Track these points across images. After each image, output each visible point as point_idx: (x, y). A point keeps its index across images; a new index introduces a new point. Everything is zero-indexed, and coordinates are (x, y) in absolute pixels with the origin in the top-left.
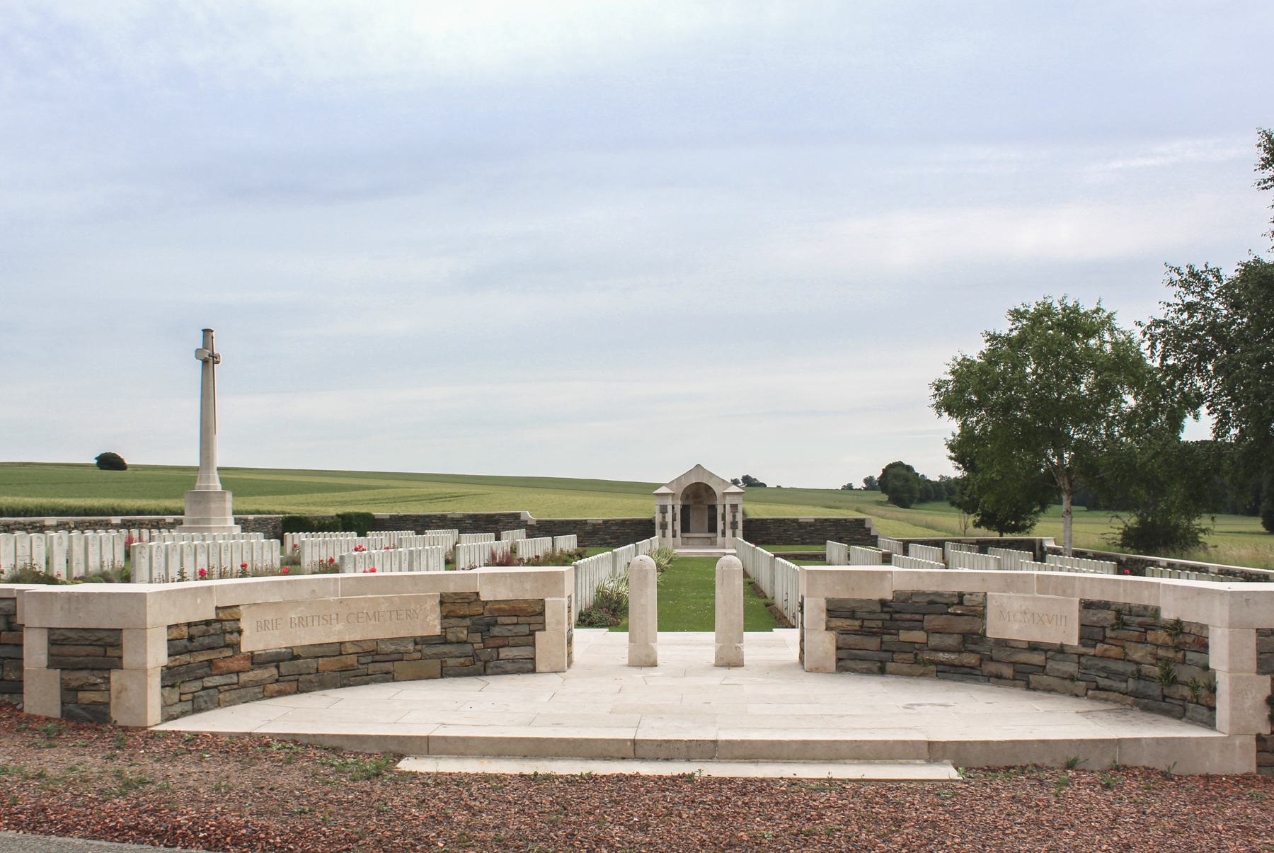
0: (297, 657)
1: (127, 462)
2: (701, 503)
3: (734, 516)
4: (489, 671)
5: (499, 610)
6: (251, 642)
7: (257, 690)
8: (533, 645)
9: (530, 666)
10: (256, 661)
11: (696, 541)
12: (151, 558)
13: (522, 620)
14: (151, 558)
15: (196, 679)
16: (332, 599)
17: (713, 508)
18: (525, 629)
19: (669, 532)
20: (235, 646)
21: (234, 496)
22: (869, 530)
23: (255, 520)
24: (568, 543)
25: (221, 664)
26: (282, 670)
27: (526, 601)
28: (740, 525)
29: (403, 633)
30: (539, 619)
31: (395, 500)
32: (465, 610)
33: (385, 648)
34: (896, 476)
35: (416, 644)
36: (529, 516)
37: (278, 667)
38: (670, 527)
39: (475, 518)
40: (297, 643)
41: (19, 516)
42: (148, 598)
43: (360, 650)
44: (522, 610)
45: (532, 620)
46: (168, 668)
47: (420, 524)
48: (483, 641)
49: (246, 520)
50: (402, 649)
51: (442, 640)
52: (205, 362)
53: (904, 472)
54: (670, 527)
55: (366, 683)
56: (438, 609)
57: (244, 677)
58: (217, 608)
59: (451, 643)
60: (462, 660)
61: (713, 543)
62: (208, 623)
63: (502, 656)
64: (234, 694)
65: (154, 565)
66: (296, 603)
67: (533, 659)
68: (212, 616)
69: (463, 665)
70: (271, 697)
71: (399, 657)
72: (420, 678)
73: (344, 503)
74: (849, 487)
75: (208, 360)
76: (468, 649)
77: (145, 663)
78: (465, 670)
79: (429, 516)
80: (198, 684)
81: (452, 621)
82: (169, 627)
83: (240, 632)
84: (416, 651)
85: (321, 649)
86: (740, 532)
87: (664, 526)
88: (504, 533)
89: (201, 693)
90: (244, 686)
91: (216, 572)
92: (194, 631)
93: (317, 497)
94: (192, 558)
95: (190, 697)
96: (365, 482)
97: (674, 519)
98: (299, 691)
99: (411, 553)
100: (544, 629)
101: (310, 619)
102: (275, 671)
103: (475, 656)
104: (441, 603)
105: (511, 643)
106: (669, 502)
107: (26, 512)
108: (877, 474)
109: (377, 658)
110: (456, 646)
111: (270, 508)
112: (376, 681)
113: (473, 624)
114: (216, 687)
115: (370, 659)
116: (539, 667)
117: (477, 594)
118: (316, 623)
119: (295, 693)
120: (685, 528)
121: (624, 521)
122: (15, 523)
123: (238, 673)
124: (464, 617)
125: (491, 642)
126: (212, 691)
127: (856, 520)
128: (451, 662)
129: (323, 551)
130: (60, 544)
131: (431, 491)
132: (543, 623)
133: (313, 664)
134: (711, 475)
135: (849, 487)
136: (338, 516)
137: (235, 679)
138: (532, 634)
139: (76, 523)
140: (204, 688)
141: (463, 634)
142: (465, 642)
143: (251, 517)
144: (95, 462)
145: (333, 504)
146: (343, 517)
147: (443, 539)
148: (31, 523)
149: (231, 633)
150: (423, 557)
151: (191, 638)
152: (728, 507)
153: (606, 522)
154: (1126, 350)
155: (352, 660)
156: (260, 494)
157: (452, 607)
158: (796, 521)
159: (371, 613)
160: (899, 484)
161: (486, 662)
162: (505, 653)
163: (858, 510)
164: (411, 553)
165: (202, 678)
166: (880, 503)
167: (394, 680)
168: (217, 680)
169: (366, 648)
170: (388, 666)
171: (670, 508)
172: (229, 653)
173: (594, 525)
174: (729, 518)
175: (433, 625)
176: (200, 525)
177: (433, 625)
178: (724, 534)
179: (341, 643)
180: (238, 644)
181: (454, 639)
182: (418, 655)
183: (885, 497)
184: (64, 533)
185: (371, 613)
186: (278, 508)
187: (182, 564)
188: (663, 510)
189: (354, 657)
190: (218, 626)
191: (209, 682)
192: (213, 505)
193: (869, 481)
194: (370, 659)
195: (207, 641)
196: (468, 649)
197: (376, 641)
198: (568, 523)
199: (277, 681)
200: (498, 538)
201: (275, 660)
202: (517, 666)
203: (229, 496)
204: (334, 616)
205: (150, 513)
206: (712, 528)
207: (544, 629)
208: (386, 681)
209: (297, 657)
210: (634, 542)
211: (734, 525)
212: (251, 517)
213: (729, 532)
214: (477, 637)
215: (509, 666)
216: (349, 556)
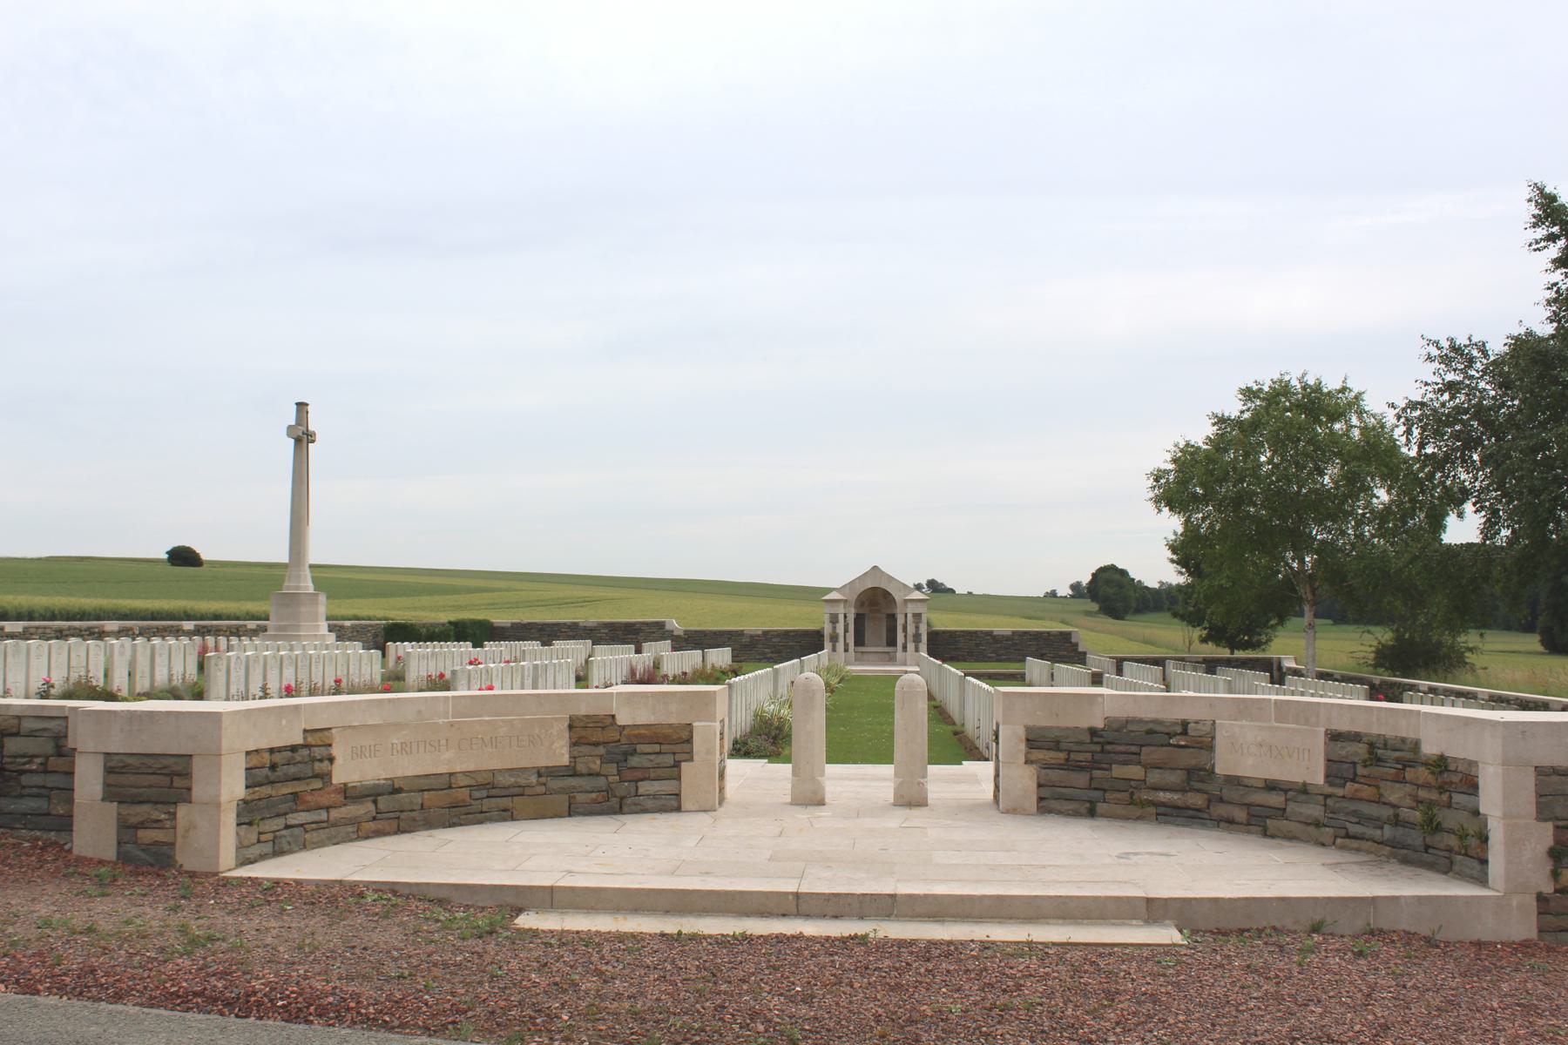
0: (398, 791)
1: (204, 557)
4: (625, 809)
5: (636, 736)
6: (347, 770)
7: (350, 829)
8: (679, 778)
9: (675, 803)
10: (349, 794)
13: (665, 748)
15: (278, 815)
18: (669, 760)
19: (840, 646)
20: (325, 777)
22: (1077, 645)
23: (353, 627)
24: (721, 657)
25: (309, 798)
26: (381, 806)
28: (924, 638)
30: (685, 747)
31: (517, 605)
32: (598, 736)
34: (1108, 582)
35: (540, 775)
36: (675, 625)
37: (375, 802)
38: (841, 639)
40: (399, 773)
42: (226, 722)
43: (472, 782)
45: (677, 748)
46: (245, 801)
47: (547, 634)
48: (619, 773)
49: (342, 627)
50: (523, 782)
51: (571, 772)
52: (298, 441)
54: (841, 639)
55: (480, 822)
56: (567, 735)
57: (334, 814)
58: (305, 731)
59: (581, 775)
60: (594, 795)
61: (892, 659)
62: (293, 748)
63: (641, 791)
64: (322, 834)
66: (399, 726)
67: (678, 795)
68: (298, 739)
69: (595, 801)
70: (367, 838)
71: (519, 791)
72: (543, 817)
74: (1053, 594)
75: (302, 438)
76: (602, 782)
80: (280, 822)
81: (583, 749)
83: (331, 760)
86: (923, 646)
87: (834, 639)
91: (305, 688)
92: (277, 758)
93: (426, 600)
97: (846, 631)
98: (400, 831)
100: (691, 759)
101: (414, 746)
102: (371, 807)
103: (609, 791)
104: (571, 727)
106: (841, 610)
107: (83, 615)
108: (1085, 579)
109: (493, 792)
111: (371, 613)
113: (608, 752)
115: (484, 793)
116: (686, 805)
120: (859, 641)
121: (787, 633)
122: (70, 628)
124: (596, 744)
125: (629, 775)
128: (580, 797)
133: (417, 798)
134: (890, 579)
135: (1053, 594)
137: (323, 815)
138: (677, 765)
140: (287, 827)
141: (596, 765)
142: (598, 774)
143: (348, 623)
147: (572, 652)
149: (321, 760)
151: (273, 767)
153: (766, 633)
155: (463, 794)
156: (358, 596)
157: (583, 733)
158: (989, 633)
159: (487, 739)
160: (1111, 591)
161: (622, 798)
162: (644, 787)
163: (1063, 622)
164: (536, 667)
166: (1089, 613)
167: (513, 819)
168: (303, 817)
169: (481, 780)
170: (505, 802)
171: (841, 617)
172: (317, 784)
174: (911, 630)
175: (561, 755)
176: (288, 633)
177: (561, 755)
178: (905, 648)
179: (451, 774)
180: (329, 774)
181: (585, 771)
182: (543, 789)
183: (1095, 607)
185: (487, 739)
186: (380, 614)
187: (265, 678)
188: (834, 619)
190: (305, 752)
191: (294, 819)
192: (303, 609)
193: (1076, 587)
194: (484, 793)
195: (292, 770)
196: (602, 782)
198: (721, 634)
199: (374, 819)
200: (638, 651)
201: (372, 793)
202: (658, 803)
203: (322, 598)
204: (443, 742)
205: (228, 618)
206: (892, 642)
207: (691, 759)
208: (505, 820)
209: (398, 791)
212: (348, 623)
213: (911, 646)
214: (612, 768)
215: (650, 803)
216: (463, 670)
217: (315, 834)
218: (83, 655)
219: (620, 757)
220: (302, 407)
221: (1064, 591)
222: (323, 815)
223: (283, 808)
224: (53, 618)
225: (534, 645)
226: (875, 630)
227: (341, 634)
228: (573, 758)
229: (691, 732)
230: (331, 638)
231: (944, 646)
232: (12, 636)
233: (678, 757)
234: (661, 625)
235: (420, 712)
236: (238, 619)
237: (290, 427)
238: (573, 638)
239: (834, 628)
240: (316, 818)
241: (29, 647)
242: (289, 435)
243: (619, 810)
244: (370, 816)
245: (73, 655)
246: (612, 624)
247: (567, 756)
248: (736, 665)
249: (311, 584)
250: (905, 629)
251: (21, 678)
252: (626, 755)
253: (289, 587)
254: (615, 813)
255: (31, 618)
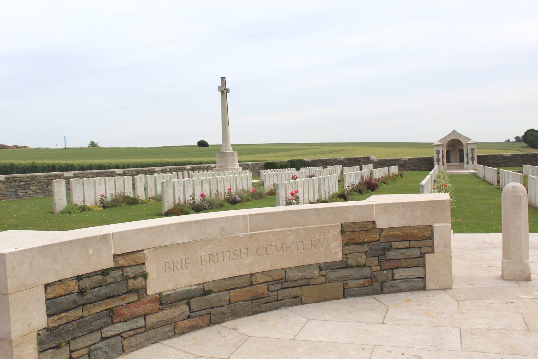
0: (210, 292)
1: (209, 144)
2: (455, 149)
3: (473, 155)
4: (385, 290)
5: (391, 236)
6: (159, 283)
7: (167, 329)
8: (424, 266)
9: (421, 285)
10: (163, 301)
11: (454, 167)
12: (174, 188)
13: (413, 244)
14: (174, 188)
15: (91, 332)
16: (241, 235)
17: (462, 151)
18: (416, 252)
19: (441, 163)
20: (141, 291)
21: (238, 155)
23: (252, 164)
24: (394, 169)
25: (125, 311)
26: (194, 307)
27: (416, 227)
28: (476, 159)
29: (309, 261)
30: (428, 242)
31: (314, 154)
32: (363, 238)
33: (291, 275)
34: (531, 135)
35: (321, 269)
36: (374, 158)
37: (189, 304)
38: (441, 160)
39: (350, 160)
40: (209, 279)
41: (143, 167)
42: (8, 259)
43: (270, 279)
44: (413, 235)
45: (422, 243)
46: (48, 329)
47: (325, 163)
48: (380, 264)
49: (248, 165)
50: (308, 275)
51: (344, 265)
52: (223, 92)
53: (535, 133)
54: (441, 160)
55: (277, 308)
56: (340, 238)
57: (151, 319)
58: (115, 256)
59: (351, 267)
60: (361, 281)
61: (462, 168)
62: (104, 272)
63: (396, 276)
64: (140, 338)
65: (176, 191)
66: (206, 242)
67: (424, 278)
68: (109, 263)
69: (362, 286)
70: (183, 333)
71: (306, 282)
72: (325, 300)
73: (293, 156)
74: (508, 141)
75: (224, 91)
76: (367, 271)
77: (9, 333)
78: (365, 290)
79: (329, 160)
80: (96, 336)
81: (352, 247)
82: (47, 286)
83: (145, 276)
84: (321, 276)
85: (232, 282)
86: (475, 162)
87: (438, 160)
88: (364, 166)
89: (100, 345)
90: (153, 328)
92: (86, 283)
93: (282, 154)
94: (200, 187)
95: (85, 351)
96: (302, 147)
97: (443, 157)
98: (211, 323)
99: (320, 179)
100: (433, 252)
101: (220, 255)
102: (185, 308)
103: (372, 278)
104: (342, 232)
105: (404, 264)
106: (440, 149)
107: (148, 165)
108: (521, 134)
109: (286, 285)
110: (356, 269)
111: (260, 159)
112: (285, 305)
113: (371, 249)
114: (119, 335)
115: (279, 286)
116: (429, 285)
117: (374, 222)
118: (227, 258)
119: (208, 325)
120: (448, 161)
121: (418, 159)
122: (141, 171)
123: (145, 316)
124: (362, 244)
125: (387, 265)
126: (113, 340)
127: (533, 154)
128: (351, 284)
129: (276, 179)
130: (141, 181)
131: (329, 149)
132: (432, 246)
133: (225, 296)
134: (461, 135)
135: (508, 141)
136: (288, 161)
137: (141, 322)
138: (422, 256)
139: (170, 169)
140: (103, 339)
141: (362, 259)
142: (364, 266)
143: (250, 163)
144: (197, 144)
145: (285, 156)
146: (290, 161)
147: (336, 169)
148: (149, 170)
149: (135, 278)
150: (327, 181)
151: (81, 292)
152: (469, 150)
153: (410, 159)
154: (194, 205)
155: (262, 289)
156: (258, 154)
157: (353, 236)
159: (279, 245)
160: (532, 138)
161: (382, 283)
162: (399, 273)
163: (519, 150)
164: (320, 179)
165: (101, 329)
166: (524, 147)
167: (302, 303)
168: (120, 327)
169: (276, 277)
170: (296, 291)
172: (133, 298)
173: (404, 161)
174: (470, 155)
175: (336, 253)
176: (223, 168)
177: (336, 253)
178: (468, 163)
179: (251, 275)
180: (145, 288)
181: (354, 263)
182: (323, 279)
183: (526, 145)
184: (142, 176)
185: (279, 245)
186: (263, 159)
187: (194, 190)
188: (438, 153)
189: (264, 286)
190: (118, 273)
191: (108, 332)
192: (229, 158)
193: (517, 138)
194: (279, 286)
195: (104, 291)
196: (367, 271)
197: (285, 270)
198: (392, 160)
199: (189, 317)
200: (361, 169)
201: (186, 297)
202: (409, 285)
203: (236, 154)
204: (244, 251)
205: (205, 163)
206: (462, 160)
207: (433, 252)
208: (296, 304)
209: (210, 292)
210: (388, 166)
211: (473, 158)
212: (250, 163)
213: (470, 162)
214: (375, 261)
215: (403, 285)
216: (282, 183)
217: (133, 339)
218: (122, 182)
219: (380, 252)
220: (223, 79)
221: (513, 140)
222: (141, 322)
223: (98, 323)
224: (137, 167)
225: (320, 168)
226: (455, 156)
227: (245, 167)
228: (345, 255)
229: (432, 231)
230: (240, 169)
231: (483, 160)
232: (119, 175)
233: (423, 250)
234: (368, 158)
235: (223, 229)
236: (209, 163)
237: (219, 87)
238: (335, 165)
239: (438, 156)
240: (134, 326)
241: (105, 179)
242: (219, 90)
243: (381, 291)
244: (184, 316)
245: (117, 183)
246: (350, 158)
247: (341, 254)
248: (400, 172)
249: (231, 149)
250: (467, 155)
251: (92, 194)
252: (384, 251)
253: (223, 150)
254: (378, 294)
255: (128, 167)
